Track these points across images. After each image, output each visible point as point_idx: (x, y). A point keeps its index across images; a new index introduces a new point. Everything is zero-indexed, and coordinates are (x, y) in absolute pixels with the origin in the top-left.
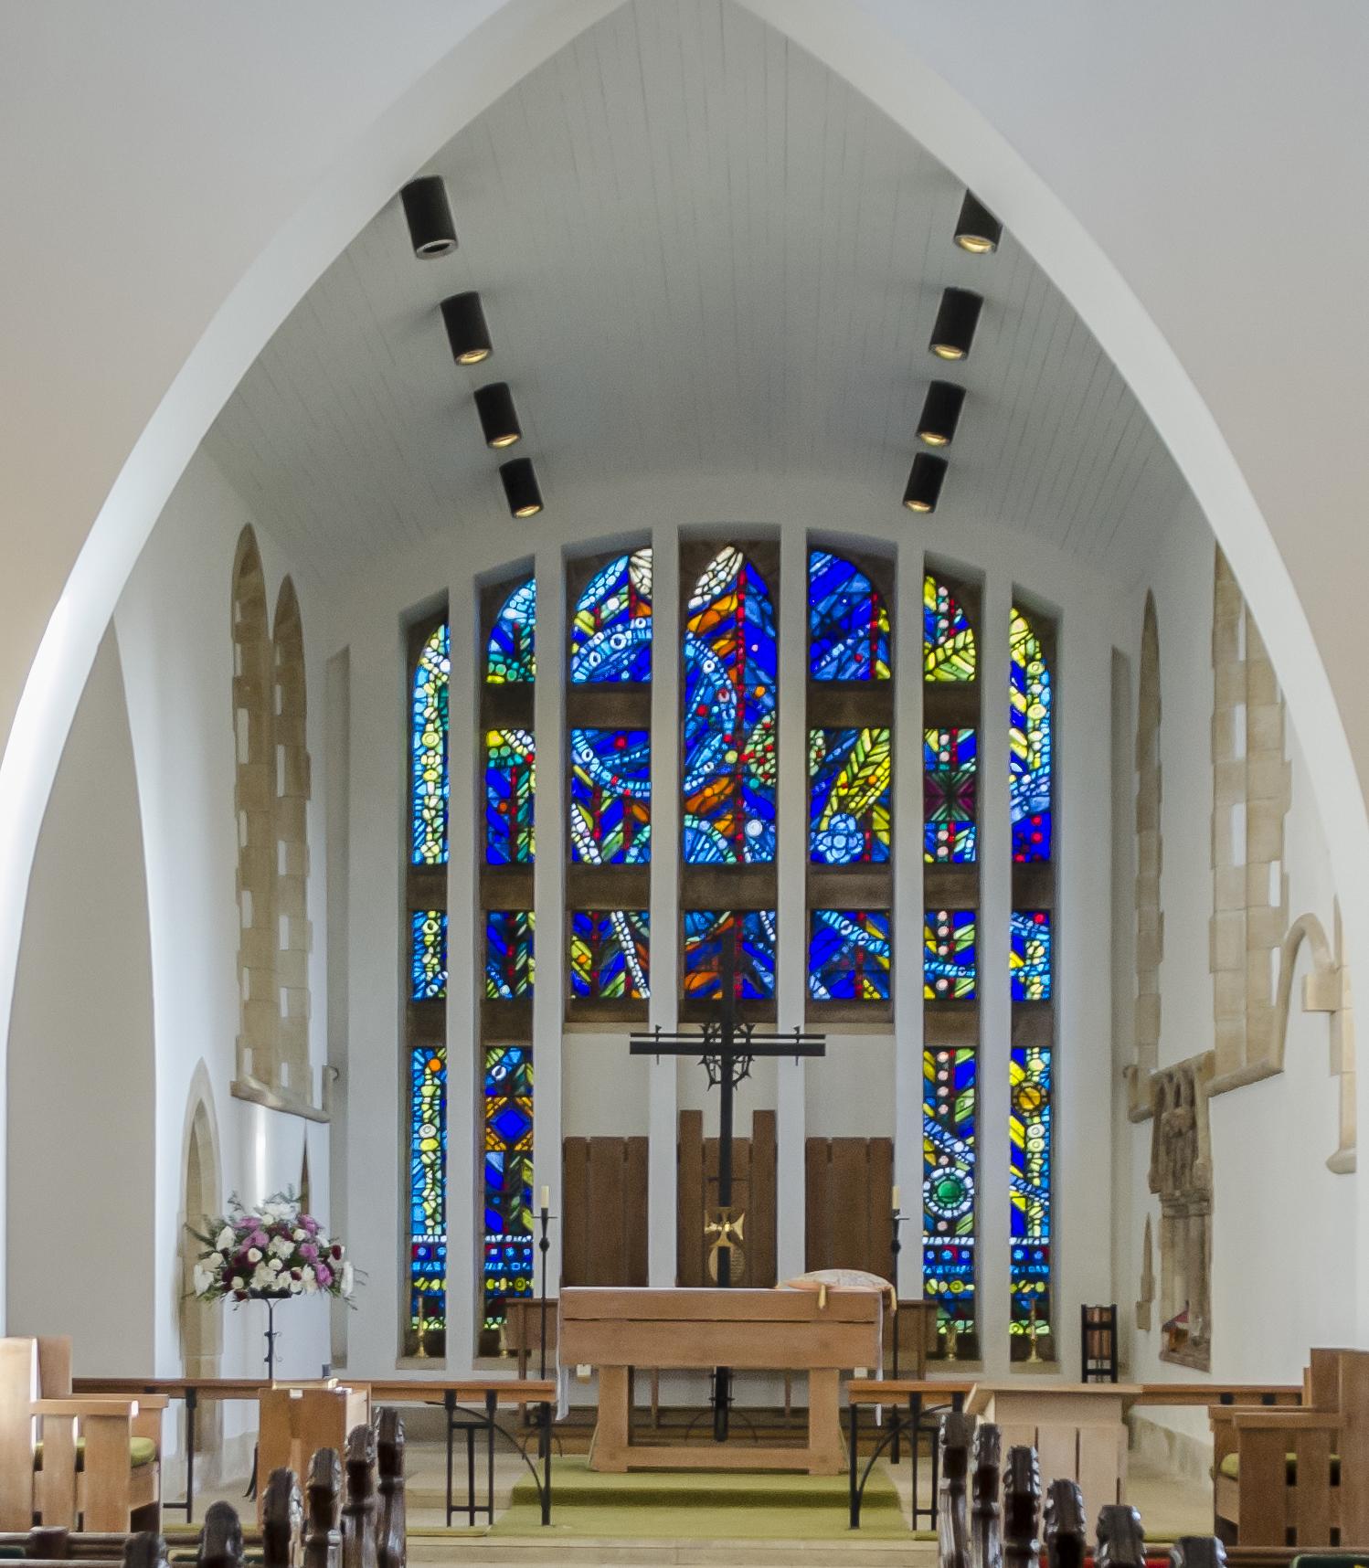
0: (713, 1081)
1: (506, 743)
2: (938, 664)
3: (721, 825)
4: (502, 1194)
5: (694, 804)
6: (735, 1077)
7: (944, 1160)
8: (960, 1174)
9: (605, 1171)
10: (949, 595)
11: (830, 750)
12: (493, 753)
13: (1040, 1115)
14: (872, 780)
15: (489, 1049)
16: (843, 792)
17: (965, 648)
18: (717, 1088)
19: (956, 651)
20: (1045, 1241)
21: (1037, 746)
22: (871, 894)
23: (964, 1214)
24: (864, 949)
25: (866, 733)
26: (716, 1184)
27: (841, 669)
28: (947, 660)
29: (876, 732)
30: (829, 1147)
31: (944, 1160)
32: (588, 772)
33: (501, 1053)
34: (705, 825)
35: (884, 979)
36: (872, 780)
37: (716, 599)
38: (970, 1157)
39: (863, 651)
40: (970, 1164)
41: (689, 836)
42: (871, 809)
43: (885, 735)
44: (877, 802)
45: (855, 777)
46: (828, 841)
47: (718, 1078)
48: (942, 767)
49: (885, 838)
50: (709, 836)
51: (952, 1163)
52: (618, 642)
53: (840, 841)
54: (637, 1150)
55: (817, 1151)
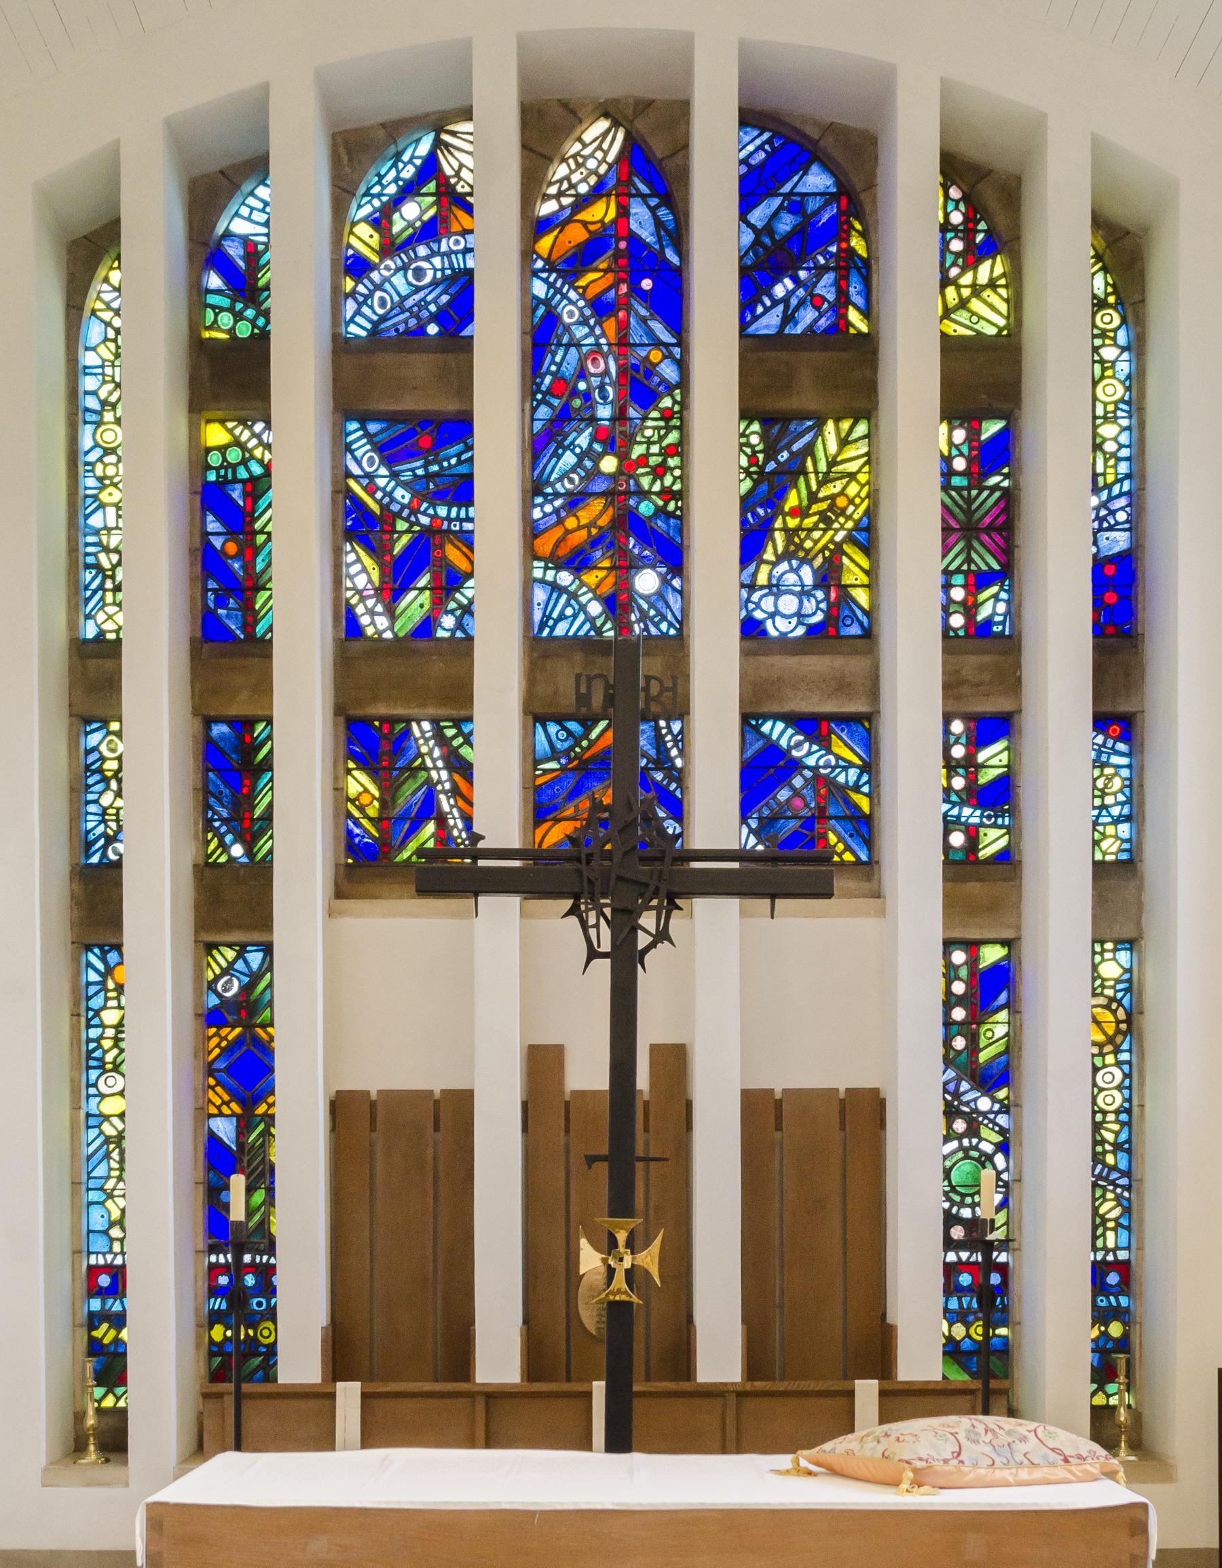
1: (237, 443)
2: (947, 313)
3: (591, 578)
5: (545, 545)
6: (643, 940)
7: (960, 1126)
8: (987, 1148)
9: (401, 1150)
10: (965, 198)
11: (771, 451)
12: (215, 459)
13: (1117, 1051)
14: (841, 502)
15: (210, 947)
16: (792, 523)
17: (992, 284)
18: (603, 967)
19: (977, 290)
20: (1122, 1255)
21: (1110, 447)
22: (842, 686)
24: (829, 782)
25: (830, 426)
26: (603, 1168)
27: (788, 319)
28: (963, 304)
29: (845, 425)
31: (960, 1126)
32: (371, 489)
33: (231, 954)
34: (565, 578)
35: (864, 827)
36: (841, 502)
37: (582, 202)
38: (1002, 1120)
39: (826, 288)
40: (1002, 1131)
41: (540, 595)
42: (838, 551)
43: (862, 428)
44: (850, 539)
45: (813, 498)
46: (768, 604)
47: (606, 946)
48: (956, 481)
49: (862, 597)
50: (574, 596)
51: (973, 1131)
53: (788, 604)
54: (452, 1114)
55: (763, 1113)
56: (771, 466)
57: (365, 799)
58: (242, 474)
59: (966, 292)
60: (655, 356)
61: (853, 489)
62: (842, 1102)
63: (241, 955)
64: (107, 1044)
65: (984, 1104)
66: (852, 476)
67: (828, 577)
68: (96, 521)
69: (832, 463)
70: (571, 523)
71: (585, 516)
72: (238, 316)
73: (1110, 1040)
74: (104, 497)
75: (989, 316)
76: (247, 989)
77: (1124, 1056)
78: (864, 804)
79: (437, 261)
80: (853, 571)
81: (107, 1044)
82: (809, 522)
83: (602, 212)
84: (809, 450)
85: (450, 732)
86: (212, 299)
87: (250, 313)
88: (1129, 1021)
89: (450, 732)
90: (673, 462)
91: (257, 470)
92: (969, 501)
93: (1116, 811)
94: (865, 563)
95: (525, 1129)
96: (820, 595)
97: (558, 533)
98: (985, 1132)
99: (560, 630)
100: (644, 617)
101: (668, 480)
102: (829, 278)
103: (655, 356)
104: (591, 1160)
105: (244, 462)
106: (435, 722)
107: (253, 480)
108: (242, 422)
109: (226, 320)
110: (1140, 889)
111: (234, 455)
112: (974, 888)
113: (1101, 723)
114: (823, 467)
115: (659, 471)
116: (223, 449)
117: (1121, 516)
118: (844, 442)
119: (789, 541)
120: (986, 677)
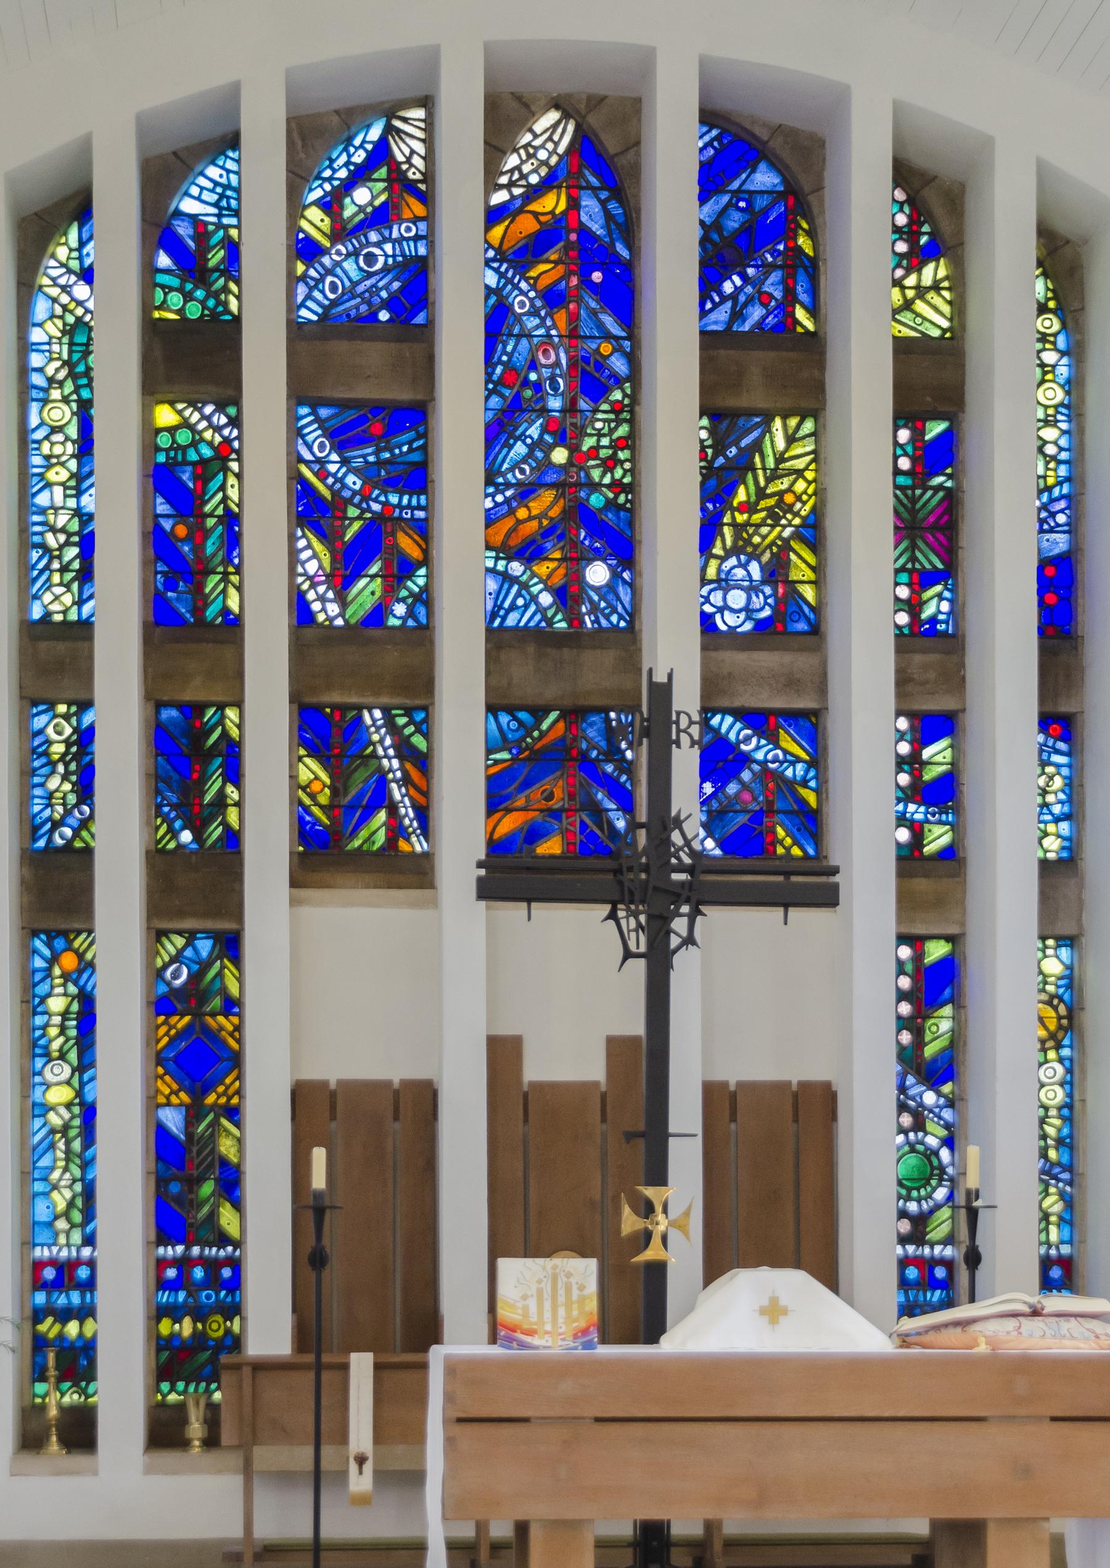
0: (628, 955)
1: (186, 424)
3: (543, 569)
4: (188, 1178)
8: (932, 1141)
14: (789, 498)
16: (741, 518)
17: (936, 287)
19: (921, 291)
23: (938, 1207)
25: (778, 423)
28: (908, 305)
29: (793, 422)
30: (333, 1095)
32: (322, 475)
33: (180, 941)
40: (948, 1126)
42: (786, 547)
43: (809, 426)
45: (761, 494)
50: (525, 586)
51: (919, 1125)
52: (371, 259)
53: (737, 598)
54: (419, 1103)
56: (721, 461)
57: (316, 787)
58: (192, 456)
59: (910, 294)
60: (606, 348)
61: (800, 486)
62: (796, 1096)
63: (189, 943)
64: (53, 1031)
65: (930, 1098)
66: (799, 473)
67: (777, 572)
68: (42, 500)
69: (780, 459)
70: (522, 513)
71: (536, 507)
72: (188, 297)
73: (1052, 1036)
74: (51, 476)
75: (933, 317)
76: (195, 978)
77: (1066, 1052)
78: (811, 798)
79: (388, 248)
80: (800, 569)
81: (53, 1031)
82: (757, 517)
83: (553, 203)
84: (757, 446)
85: (401, 721)
86: (161, 278)
87: (200, 294)
88: (1070, 1016)
89: (401, 721)
90: (622, 455)
91: (207, 452)
92: (914, 500)
93: (1057, 809)
94: (811, 559)
95: (293, 1119)
96: (768, 590)
97: (509, 523)
98: (930, 1126)
99: (511, 620)
100: (594, 609)
101: (618, 473)
102: (775, 276)
103: (606, 348)
104: (630, 1136)
105: (194, 444)
106: (386, 711)
107: (203, 462)
108: (192, 404)
109: (176, 300)
110: (1081, 886)
111: (184, 437)
112: (921, 884)
113: (1046, 722)
114: (771, 463)
115: (610, 464)
116: (172, 430)
117: (1061, 518)
118: (791, 440)
119: (737, 536)
120: (932, 675)
